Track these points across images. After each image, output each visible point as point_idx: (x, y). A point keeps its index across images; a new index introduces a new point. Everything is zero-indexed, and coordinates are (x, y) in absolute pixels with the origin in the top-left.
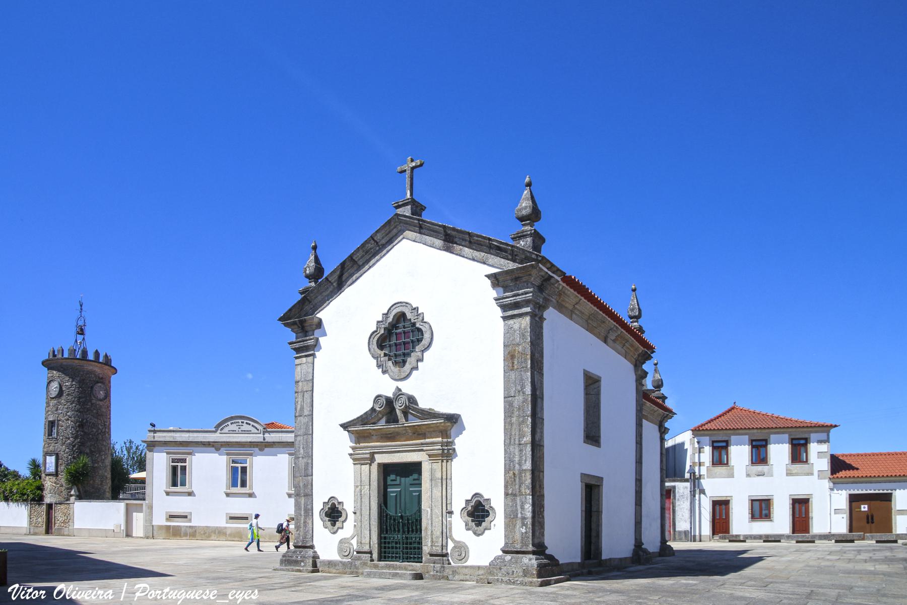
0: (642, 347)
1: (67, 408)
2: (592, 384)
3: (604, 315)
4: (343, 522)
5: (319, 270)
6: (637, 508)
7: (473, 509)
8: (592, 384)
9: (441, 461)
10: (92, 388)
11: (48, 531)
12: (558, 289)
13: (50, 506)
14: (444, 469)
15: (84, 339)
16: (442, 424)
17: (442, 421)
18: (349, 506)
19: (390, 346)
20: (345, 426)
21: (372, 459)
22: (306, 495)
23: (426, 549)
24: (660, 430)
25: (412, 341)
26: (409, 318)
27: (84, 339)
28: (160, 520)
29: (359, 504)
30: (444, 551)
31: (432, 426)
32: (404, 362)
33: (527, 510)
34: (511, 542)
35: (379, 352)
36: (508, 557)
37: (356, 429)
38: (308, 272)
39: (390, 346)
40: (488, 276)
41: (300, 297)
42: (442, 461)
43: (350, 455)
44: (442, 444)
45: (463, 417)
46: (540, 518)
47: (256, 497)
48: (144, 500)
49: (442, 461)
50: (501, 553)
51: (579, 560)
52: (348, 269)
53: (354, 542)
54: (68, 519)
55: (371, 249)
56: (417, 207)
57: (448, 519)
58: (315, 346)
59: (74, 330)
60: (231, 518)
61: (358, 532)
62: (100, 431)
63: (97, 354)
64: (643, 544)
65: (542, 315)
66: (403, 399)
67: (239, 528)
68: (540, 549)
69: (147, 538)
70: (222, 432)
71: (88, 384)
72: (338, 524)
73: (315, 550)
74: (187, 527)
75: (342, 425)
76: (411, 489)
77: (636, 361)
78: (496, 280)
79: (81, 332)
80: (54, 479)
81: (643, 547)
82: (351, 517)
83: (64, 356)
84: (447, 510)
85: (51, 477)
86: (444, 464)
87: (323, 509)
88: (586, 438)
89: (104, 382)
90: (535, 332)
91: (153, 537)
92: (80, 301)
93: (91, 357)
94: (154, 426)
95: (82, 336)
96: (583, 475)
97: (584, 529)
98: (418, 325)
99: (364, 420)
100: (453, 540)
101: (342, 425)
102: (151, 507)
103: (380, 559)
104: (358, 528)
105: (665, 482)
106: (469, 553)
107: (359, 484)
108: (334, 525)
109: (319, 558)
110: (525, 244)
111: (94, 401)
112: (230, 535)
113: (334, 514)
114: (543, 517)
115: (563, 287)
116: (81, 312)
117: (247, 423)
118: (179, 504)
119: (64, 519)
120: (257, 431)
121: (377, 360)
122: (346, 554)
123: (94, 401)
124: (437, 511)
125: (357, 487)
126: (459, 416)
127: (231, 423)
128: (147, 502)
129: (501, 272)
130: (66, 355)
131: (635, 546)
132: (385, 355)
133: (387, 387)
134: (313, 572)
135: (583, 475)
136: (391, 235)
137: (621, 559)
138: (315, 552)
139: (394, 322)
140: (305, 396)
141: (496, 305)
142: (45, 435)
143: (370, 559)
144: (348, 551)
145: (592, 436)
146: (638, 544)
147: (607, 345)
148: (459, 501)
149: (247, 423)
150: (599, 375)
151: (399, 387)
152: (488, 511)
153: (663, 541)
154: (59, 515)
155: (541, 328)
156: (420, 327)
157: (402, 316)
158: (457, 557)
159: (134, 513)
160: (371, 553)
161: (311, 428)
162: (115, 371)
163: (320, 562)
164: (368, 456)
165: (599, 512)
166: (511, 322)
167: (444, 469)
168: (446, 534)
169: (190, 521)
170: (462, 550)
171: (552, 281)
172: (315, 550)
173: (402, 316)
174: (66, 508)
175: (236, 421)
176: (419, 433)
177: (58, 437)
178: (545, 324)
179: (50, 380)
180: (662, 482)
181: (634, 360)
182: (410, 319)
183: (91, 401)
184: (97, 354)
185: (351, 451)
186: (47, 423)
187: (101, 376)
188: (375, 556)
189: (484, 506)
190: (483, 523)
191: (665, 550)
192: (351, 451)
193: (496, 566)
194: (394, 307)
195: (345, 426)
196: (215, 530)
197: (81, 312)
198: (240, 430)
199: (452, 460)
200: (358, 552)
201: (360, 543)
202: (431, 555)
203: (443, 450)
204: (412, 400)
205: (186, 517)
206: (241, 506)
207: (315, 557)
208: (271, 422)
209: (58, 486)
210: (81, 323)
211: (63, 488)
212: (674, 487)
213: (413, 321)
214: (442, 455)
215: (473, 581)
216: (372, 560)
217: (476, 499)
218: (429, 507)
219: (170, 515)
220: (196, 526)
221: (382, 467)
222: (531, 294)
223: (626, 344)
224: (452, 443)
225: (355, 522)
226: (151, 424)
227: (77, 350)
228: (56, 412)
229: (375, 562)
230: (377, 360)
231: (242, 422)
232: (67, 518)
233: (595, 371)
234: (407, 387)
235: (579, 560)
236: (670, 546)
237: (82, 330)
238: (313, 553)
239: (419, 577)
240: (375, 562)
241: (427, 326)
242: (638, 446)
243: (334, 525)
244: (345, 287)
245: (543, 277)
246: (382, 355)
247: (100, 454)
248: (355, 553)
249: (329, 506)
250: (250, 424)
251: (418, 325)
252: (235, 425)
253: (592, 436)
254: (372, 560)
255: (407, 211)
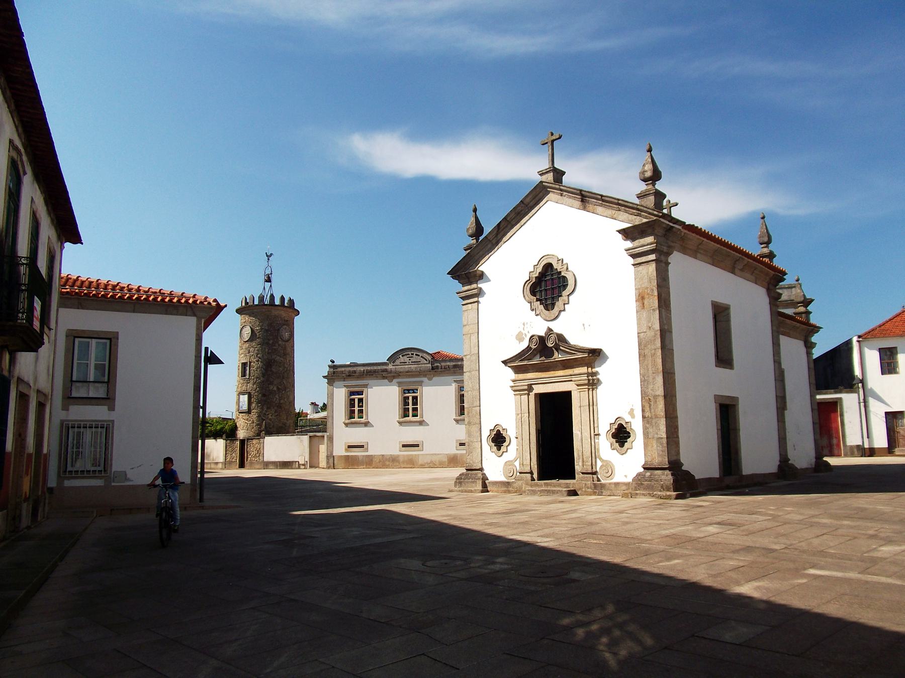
0: (772, 272)
1: (258, 350)
2: (721, 314)
3: (728, 250)
4: (507, 446)
5: (479, 229)
6: (780, 425)
7: (616, 431)
8: (721, 314)
9: (587, 390)
10: (278, 330)
11: (242, 465)
12: (681, 235)
13: (243, 442)
14: (591, 397)
15: (271, 286)
16: (588, 358)
17: (587, 355)
18: (511, 432)
19: (541, 291)
20: (505, 362)
21: (530, 388)
22: (645, 380)
23: (578, 467)
24: (806, 346)
25: (559, 287)
26: (555, 267)
27: (271, 286)
28: (339, 450)
29: (855, 519)
30: (594, 470)
31: (579, 359)
32: (553, 305)
33: (663, 431)
34: (650, 460)
35: (532, 297)
36: (648, 474)
37: (516, 364)
38: (470, 231)
39: (541, 291)
40: (619, 231)
41: (465, 253)
42: (589, 389)
43: (512, 387)
44: (588, 374)
45: (604, 349)
46: (675, 438)
47: (428, 425)
48: (326, 432)
49: (589, 389)
50: (642, 470)
51: (718, 476)
52: (504, 229)
53: (517, 464)
54: (260, 452)
55: (521, 211)
56: (558, 173)
57: (596, 441)
58: (479, 294)
59: (263, 278)
60: (404, 446)
61: (520, 456)
62: (286, 369)
63: (282, 298)
64: (790, 460)
65: (667, 260)
66: (553, 337)
67: (411, 455)
68: (675, 466)
69: (329, 468)
70: (395, 364)
71: (276, 327)
72: (503, 449)
73: (484, 472)
74: (364, 456)
75: (503, 362)
76: (818, 397)
77: (768, 284)
78: (627, 234)
79: (269, 280)
80: (245, 416)
81: (790, 462)
82: (514, 441)
83: (255, 303)
84: (594, 432)
85: (244, 414)
86: (591, 392)
87: (490, 435)
88: (718, 362)
89: (290, 325)
90: (661, 276)
91: (334, 467)
92: (266, 253)
93: (277, 302)
94: (333, 362)
95: (270, 283)
96: (717, 397)
97: (721, 447)
98: (563, 274)
99: (520, 356)
100: (601, 459)
101: (503, 362)
102: (331, 439)
103: (540, 478)
104: (520, 451)
105: (815, 396)
106: (614, 470)
107: (519, 412)
108: (499, 449)
109: (488, 480)
110: (650, 201)
111: (280, 342)
112: (403, 462)
113: (499, 439)
114: (678, 437)
115: (685, 233)
116: (268, 262)
117: (416, 355)
118: (357, 435)
119: (255, 454)
120: (425, 362)
121: (531, 304)
122: (511, 474)
123: (280, 342)
124: (586, 434)
125: (518, 414)
126: (601, 350)
127: (402, 356)
128: (328, 434)
129: (630, 227)
130: (256, 302)
131: (780, 461)
132: (537, 300)
133: (539, 327)
134: (482, 492)
135: (717, 397)
136: (537, 199)
137: (764, 475)
138: (484, 474)
139: (543, 272)
140: (472, 337)
141: (627, 255)
142: (238, 376)
143: (530, 478)
144: (512, 472)
145: (724, 358)
146: (784, 461)
147: (735, 275)
148: (605, 426)
149: (416, 355)
150: (728, 303)
151: (550, 327)
152: (629, 433)
153: (819, 457)
154: (251, 448)
155: (667, 270)
156: (565, 275)
157: (549, 267)
158: (605, 474)
159: (65, 485)
160: (531, 473)
161: (478, 364)
162: (298, 313)
163: (489, 482)
164: (526, 387)
165: (736, 430)
166: (640, 268)
167: (591, 397)
168: (594, 454)
169: (367, 450)
170: (609, 468)
171: (674, 229)
172: (484, 472)
173: (549, 267)
174: (257, 443)
175: (406, 353)
176: (566, 365)
177: (250, 377)
178: (670, 267)
179: (243, 325)
180: (812, 396)
181: (766, 284)
182: (557, 269)
183: (278, 342)
184: (282, 298)
185: (512, 384)
186: (241, 365)
187: (286, 319)
188: (535, 476)
189: (626, 428)
190: (626, 443)
191: (821, 466)
192: (512, 384)
193: (639, 478)
194: (540, 262)
195: (505, 362)
196: (389, 458)
197: (268, 262)
198: (410, 361)
199: (597, 388)
200: (520, 473)
201: (522, 464)
202: (583, 473)
203: (589, 380)
204: (561, 338)
205: (362, 446)
206: (411, 434)
207: (484, 479)
208: (437, 351)
209: (250, 422)
210: (268, 272)
211: (255, 424)
212: (840, 399)
213: (559, 270)
214: (588, 384)
215: (620, 496)
216: (533, 479)
217: (619, 422)
218: (580, 431)
219: (348, 446)
220: (372, 455)
221: (538, 396)
222: (655, 245)
223: (755, 271)
224: (595, 374)
225: (517, 446)
226: (331, 361)
227: (265, 296)
228: (248, 355)
229: (536, 481)
230: (531, 304)
231: (412, 354)
232: (258, 453)
233: (722, 300)
234: (558, 327)
235: (718, 476)
236: (826, 462)
237: (269, 277)
238: (482, 475)
239: (573, 493)
240: (536, 481)
241: (571, 274)
242: (777, 365)
243: (499, 449)
244: (502, 242)
245: (665, 228)
246: (535, 300)
247: (285, 390)
248: (518, 474)
249: (495, 433)
250: (419, 356)
251: (563, 274)
252: (405, 357)
253: (724, 358)
254: (533, 479)
255: (550, 177)
